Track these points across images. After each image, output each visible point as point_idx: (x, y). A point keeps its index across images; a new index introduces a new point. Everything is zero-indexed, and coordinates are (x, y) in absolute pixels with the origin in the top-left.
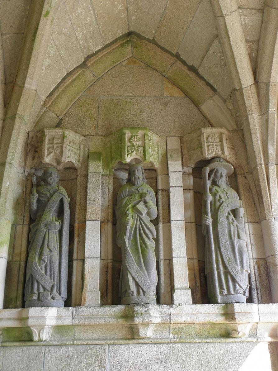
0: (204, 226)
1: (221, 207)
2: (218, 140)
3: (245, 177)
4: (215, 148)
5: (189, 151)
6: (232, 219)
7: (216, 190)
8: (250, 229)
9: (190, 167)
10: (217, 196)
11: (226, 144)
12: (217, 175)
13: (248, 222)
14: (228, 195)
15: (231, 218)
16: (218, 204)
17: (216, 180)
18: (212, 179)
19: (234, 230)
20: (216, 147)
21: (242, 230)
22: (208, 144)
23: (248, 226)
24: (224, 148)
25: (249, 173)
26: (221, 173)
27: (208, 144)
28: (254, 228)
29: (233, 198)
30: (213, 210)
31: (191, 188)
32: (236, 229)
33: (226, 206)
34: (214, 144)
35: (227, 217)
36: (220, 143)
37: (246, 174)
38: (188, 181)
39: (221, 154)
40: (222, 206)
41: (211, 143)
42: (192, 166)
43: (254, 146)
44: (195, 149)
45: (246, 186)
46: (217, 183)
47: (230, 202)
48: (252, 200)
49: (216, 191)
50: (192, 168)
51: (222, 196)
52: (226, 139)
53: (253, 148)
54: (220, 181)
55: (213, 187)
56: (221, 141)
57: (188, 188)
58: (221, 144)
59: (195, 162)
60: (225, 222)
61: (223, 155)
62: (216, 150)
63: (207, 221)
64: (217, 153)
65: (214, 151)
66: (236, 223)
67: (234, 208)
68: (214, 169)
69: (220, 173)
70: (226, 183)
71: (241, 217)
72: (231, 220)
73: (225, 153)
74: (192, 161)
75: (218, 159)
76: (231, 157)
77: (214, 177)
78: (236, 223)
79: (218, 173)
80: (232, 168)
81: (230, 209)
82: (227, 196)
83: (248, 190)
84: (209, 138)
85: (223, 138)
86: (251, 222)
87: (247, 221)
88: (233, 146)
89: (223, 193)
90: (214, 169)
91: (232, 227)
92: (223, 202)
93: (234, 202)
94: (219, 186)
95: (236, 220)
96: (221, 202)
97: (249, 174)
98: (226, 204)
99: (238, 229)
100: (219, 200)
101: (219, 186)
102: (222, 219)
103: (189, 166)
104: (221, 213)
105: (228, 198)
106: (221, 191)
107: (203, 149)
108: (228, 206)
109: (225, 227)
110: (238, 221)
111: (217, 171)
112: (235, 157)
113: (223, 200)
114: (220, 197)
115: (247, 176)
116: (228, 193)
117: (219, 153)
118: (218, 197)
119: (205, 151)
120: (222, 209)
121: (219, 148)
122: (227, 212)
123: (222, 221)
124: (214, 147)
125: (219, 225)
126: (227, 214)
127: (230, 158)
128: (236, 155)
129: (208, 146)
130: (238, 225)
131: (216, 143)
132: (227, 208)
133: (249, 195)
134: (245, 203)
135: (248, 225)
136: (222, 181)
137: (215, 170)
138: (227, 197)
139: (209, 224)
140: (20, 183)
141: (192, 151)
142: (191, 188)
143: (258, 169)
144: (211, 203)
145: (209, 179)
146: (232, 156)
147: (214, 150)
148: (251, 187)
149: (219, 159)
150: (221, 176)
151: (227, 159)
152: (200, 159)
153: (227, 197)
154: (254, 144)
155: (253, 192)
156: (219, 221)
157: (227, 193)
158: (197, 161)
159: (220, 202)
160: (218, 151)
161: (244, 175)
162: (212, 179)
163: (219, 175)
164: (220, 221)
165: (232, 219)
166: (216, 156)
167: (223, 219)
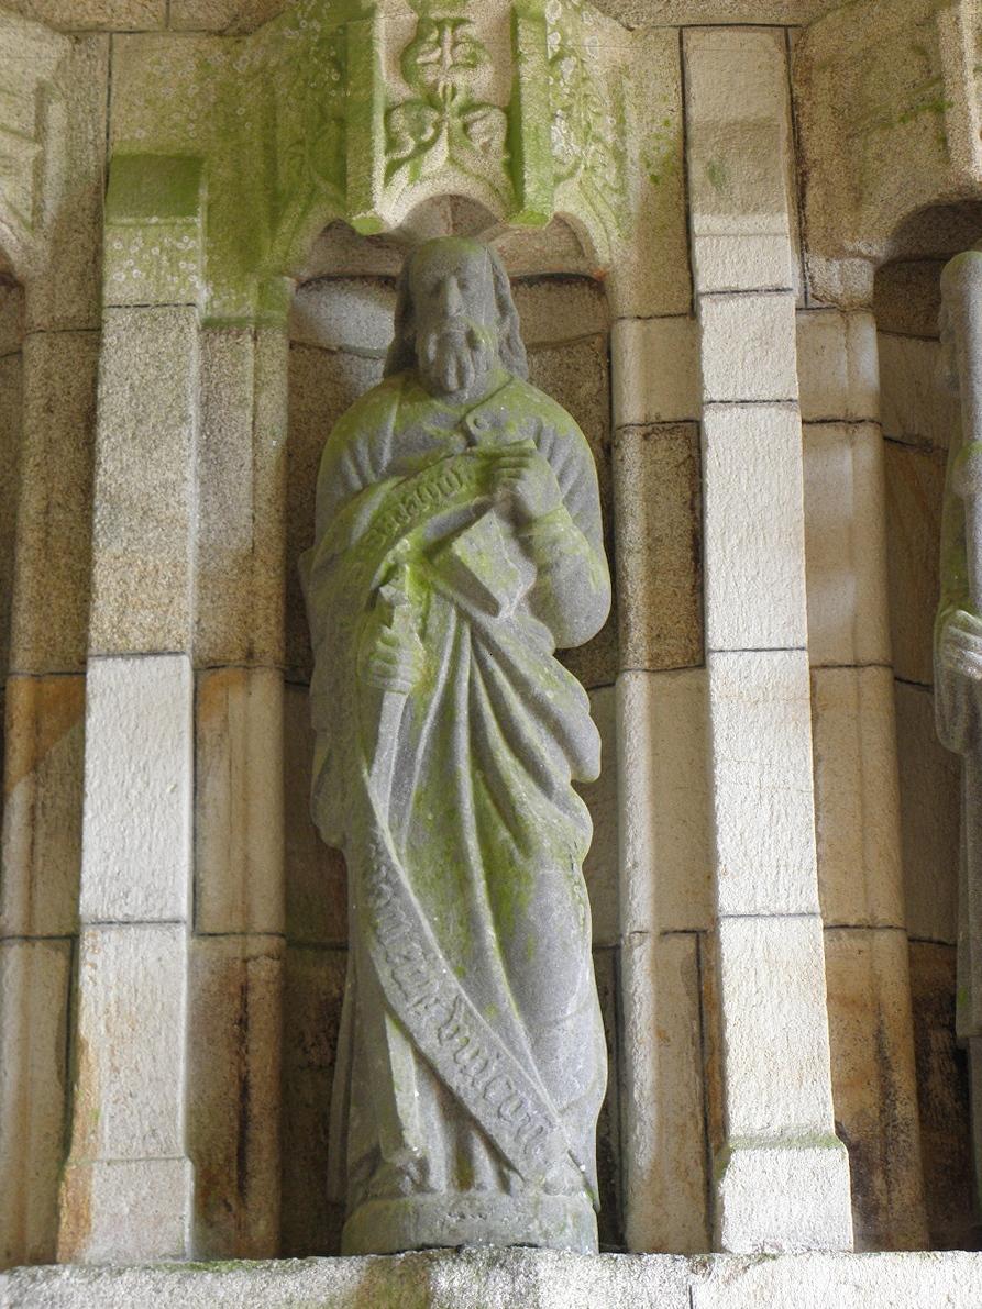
0: (953, 691)
5: (849, 137)
9: (859, 255)
31: (862, 414)
50: (873, 260)
57: (840, 414)
59: (891, 223)
63: (973, 655)
74: (871, 212)
103: (849, 246)
107: (951, 116)
141: (876, 136)
142: (866, 409)
152: (929, 197)
158: (910, 207)
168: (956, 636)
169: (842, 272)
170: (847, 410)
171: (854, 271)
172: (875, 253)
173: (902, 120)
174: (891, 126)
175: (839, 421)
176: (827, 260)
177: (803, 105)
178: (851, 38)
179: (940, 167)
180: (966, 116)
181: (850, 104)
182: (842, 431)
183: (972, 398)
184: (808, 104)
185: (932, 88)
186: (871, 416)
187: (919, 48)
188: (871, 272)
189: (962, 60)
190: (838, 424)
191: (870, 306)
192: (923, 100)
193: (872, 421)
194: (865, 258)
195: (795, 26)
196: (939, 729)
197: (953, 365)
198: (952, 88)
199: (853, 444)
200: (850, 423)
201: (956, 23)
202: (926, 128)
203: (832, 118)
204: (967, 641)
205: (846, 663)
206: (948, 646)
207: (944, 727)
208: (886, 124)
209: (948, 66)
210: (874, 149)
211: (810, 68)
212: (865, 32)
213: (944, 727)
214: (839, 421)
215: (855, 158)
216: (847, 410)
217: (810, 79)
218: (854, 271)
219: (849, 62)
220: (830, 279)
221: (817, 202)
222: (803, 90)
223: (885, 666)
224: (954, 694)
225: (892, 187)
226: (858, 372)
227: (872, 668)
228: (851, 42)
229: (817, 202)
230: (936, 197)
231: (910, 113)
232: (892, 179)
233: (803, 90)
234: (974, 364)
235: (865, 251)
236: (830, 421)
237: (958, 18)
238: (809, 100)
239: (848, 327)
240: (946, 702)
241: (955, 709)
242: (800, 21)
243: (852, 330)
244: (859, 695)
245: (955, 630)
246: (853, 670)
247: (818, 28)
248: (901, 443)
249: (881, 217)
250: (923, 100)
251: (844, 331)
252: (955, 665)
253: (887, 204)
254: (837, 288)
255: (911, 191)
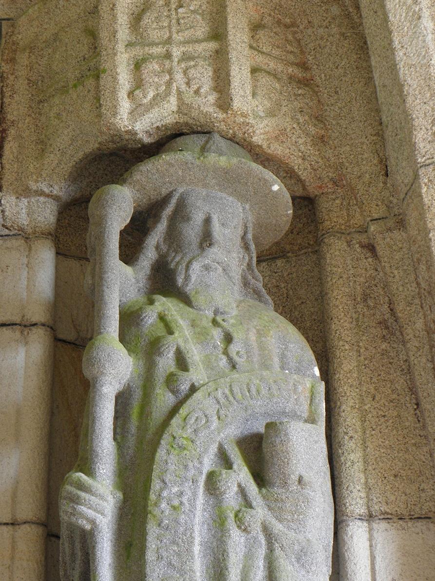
0: (71, 538)
1: (175, 421)
2: (202, 29)
3: (371, 248)
4: (179, 77)
5: (40, 102)
6: (242, 491)
7: (162, 318)
8: (378, 559)
9: (42, 193)
10: (160, 354)
11: (247, 51)
12: (180, 233)
13: (370, 517)
14: (233, 349)
15: (235, 489)
16: (164, 399)
17: (174, 260)
18: (149, 255)
19: (249, 556)
20: (185, 72)
21: (298, 560)
22: (138, 51)
23: (371, 539)
24: (228, 75)
25: (391, 223)
26: (208, 221)
27: (138, 51)
28: (405, 553)
29: (265, 365)
30: (132, 441)
31: (34, 320)
32: (262, 552)
33: (212, 411)
34: (176, 52)
35: (212, 483)
36: (212, 45)
37: (372, 228)
38: (25, 274)
39: (211, 110)
40: (183, 411)
41: (157, 44)
42: (56, 191)
43: (399, 54)
44: (71, 85)
45: (371, 303)
46: (180, 281)
47: (236, 390)
48: (401, 383)
49: (161, 325)
50: (56, 198)
51: (195, 354)
52: (256, 27)
53: (393, 68)
54: (196, 266)
55: (151, 302)
56: (218, 34)
57: (17, 319)
58: (217, 52)
59: (67, 167)
60: (192, 511)
61: (221, 116)
62: (183, 87)
63: (83, 509)
64: (190, 107)
65: (168, 93)
66: (260, 512)
67: (259, 427)
68: (164, 202)
69: (198, 218)
70: (246, 284)
71: (294, 478)
72: (231, 499)
73: (237, 104)
74: (52, 159)
75: (197, 141)
76: (283, 132)
77: (164, 248)
78: (260, 512)
79: (188, 219)
80: (276, 188)
81: (232, 431)
82: (226, 352)
83: (383, 323)
84: (147, 20)
85: (230, 17)
86: (387, 517)
87: (363, 510)
88: (304, 66)
89: (202, 336)
90: (164, 202)
91: (236, 540)
92: (193, 389)
93: (264, 392)
94: (186, 299)
95: (264, 497)
96: (184, 387)
97: (390, 230)
98: (210, 401)
99: (271, 549)
100: (171, 381)
101: (186, 299)
102: (175, 489)
103: (33, 186)
104: (173, 458)
105: (234, 366)
106: (193, 325)
107: (105, 80)
108: (222, 412)
109: (191, 543)
110: (274, 506)
111: (181, 213)
112: (312, 130)
113: (197, 374)
114: (182, 362)
115: (379, 238)
116: (235, 335)
117: (200, 100)
118: (166, 363)
119: (114, 92)
120: (178, 432)
121: (204, 76)
122: (214, 449)
123: (176, 503)
124: (170, 72)
125: (152, 530)
126: (208, 463)
127: (281, 135)
128: (319, 119)
129: (138, 66)
130: (278, 527)
131: (189, 48)
132: (215, 423)
133: (384, 353)
134: (362, 402)
135: (371, 530)
136: (207, 268)
137: (174, 201)
138: (230, 359)
139: (93, 522)
140: (35, 447)
141: (57, 100)
142: (38, 314)
143: (424, 190)
144: (122, 400)
145: (129, 254)
146: (287, 123)
147: (169, 84)
148: (400, 307)
149: (203, 139)
150: (206, 239)
151: (257, 139)
152: (92, 146)
153: (223, 362)
154: (396, 44)
155: (409, 332)
156: (156, 504)
157: (228, 339)
158: (80, 155)
159: (174, 392)
160: (197, 92)
161: (363, 238)
162: (149, 255)
163: (191, 232)
164: (163, 505)
165: (242, 491)
166: (187, 124)
167: (181, 494)
168: (71, 493)
169: (29, 207)
170: (23, 316)
171: (38, 207)
172: (55, 192)
173: (75, 86)
174: (67, 91)
175: (16, 324)
176: (17, 198)
177: (8, 78)
178: (46, 27)
179: (96, 121)
180: (115, 79)
181: (43, 77)
182: (18, 333)
183: (101, 300)
184: (12, 78)
185: (95, 60)
186: (43, 320)
187: (89, 31)
188: (55, 208)
189: (115, 36)
190: (14, 327)
191: (51, 235)
192: (89, 70)
193: (43, 325)
194: (48, 196)
195: (8, 19)
196: (61, 573)
197: (93, 277)
198: (106, 58)
199: (27, 343)
200: (25, 326)
201: (112, 9)
202: (89, 91)
203: (27, 87)
204: (78, 497)
205: (5, 521)
206: (65, 502)
207: (65, 571)
208: (64, 90)
209: (105, 42)
210: (55, 110)
211: (15, 51)
212: (55, 21)
213: (65, 571)
214: (16, 324)
215: (43, 119)
216: (23, 316)
217: (14, 59)
218: (38, 207)
219: (44, 45)
220: (18, 213)
221: (12, 153)
222: (8, 67)
223: (38, 524)
224: (72, 543)
225: (66, 139)
226: (35, 286)
227: (27, 526)
228: (46, 29)
229: (12, 153)
230: (97, 145)
231: (80, 80)
232: (66, 132)
233: (8, 67)
234: (105, 272)
235: (47, 190)
236: (9, 325)
237: (114, 5)
238: (12, 74)
239: (30, 250)
240: (67, 550)
241: (73, 554)
242: (12, 15)
243: (33, 252)
244: (13, 549)
245: (69, 488)
246: (10, 527)
247: (23, 20)
248: (74, 344)
249: (59, 163)
250: (89, 70)
251: (27, 253)
252: (69, 517)
253: (63, 153)
254: (24, 220)
255: (80, 142)
